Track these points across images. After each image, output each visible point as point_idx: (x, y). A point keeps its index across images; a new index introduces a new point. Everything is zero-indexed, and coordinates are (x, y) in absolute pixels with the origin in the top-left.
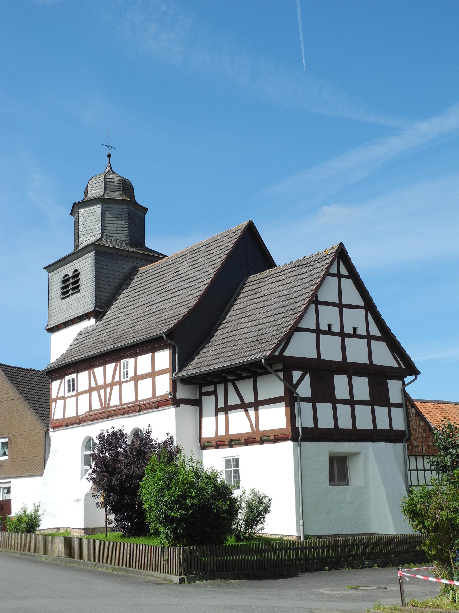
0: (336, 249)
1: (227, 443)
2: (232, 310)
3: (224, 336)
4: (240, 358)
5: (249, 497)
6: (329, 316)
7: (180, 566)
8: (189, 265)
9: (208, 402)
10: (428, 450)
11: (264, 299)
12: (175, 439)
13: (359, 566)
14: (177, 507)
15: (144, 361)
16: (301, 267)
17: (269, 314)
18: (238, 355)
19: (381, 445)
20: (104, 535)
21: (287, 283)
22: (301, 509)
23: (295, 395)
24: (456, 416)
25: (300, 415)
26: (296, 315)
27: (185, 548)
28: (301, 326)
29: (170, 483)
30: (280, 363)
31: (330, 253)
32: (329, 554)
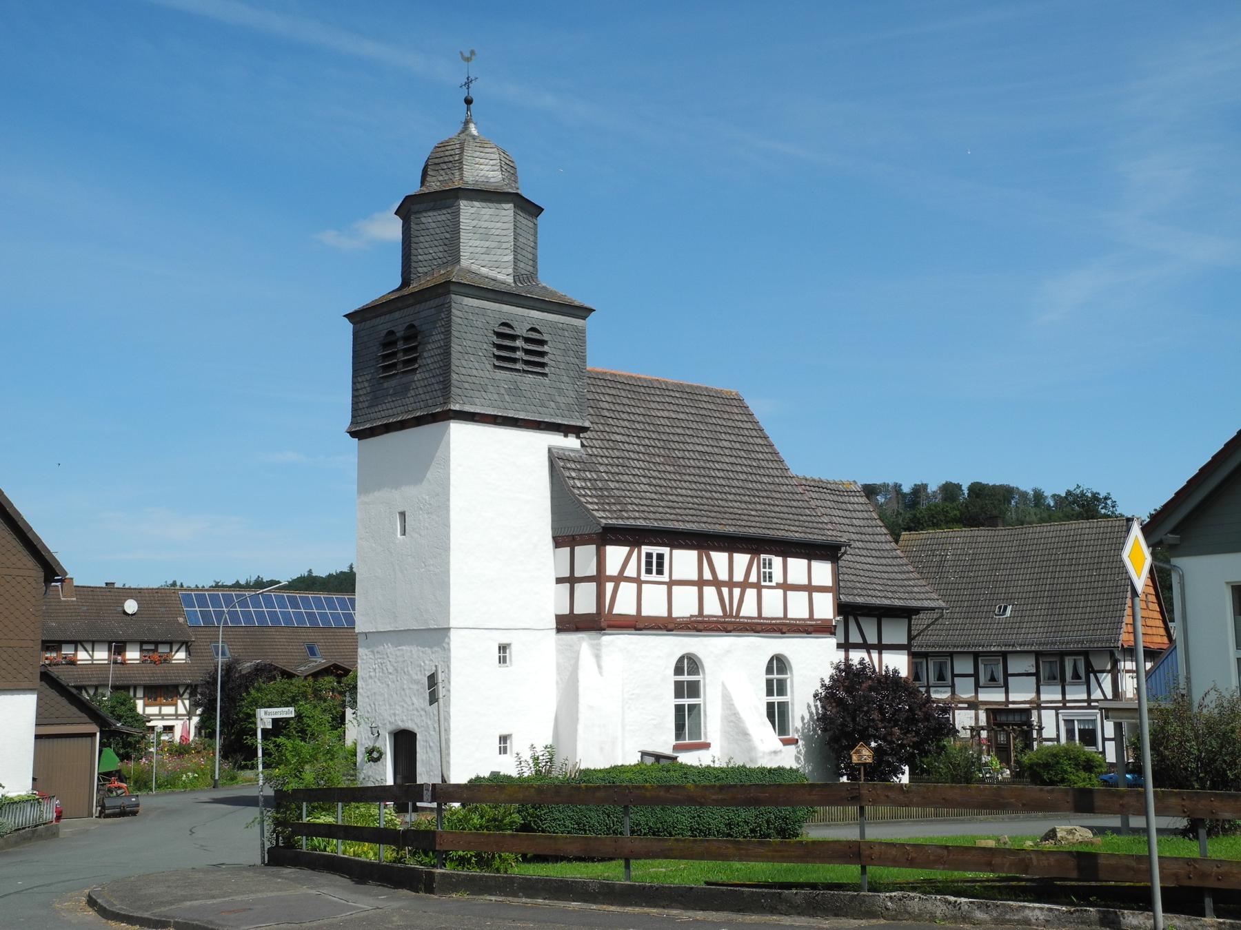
15: (797, 568)
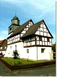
15: (17, 36)
20: (34, 42)
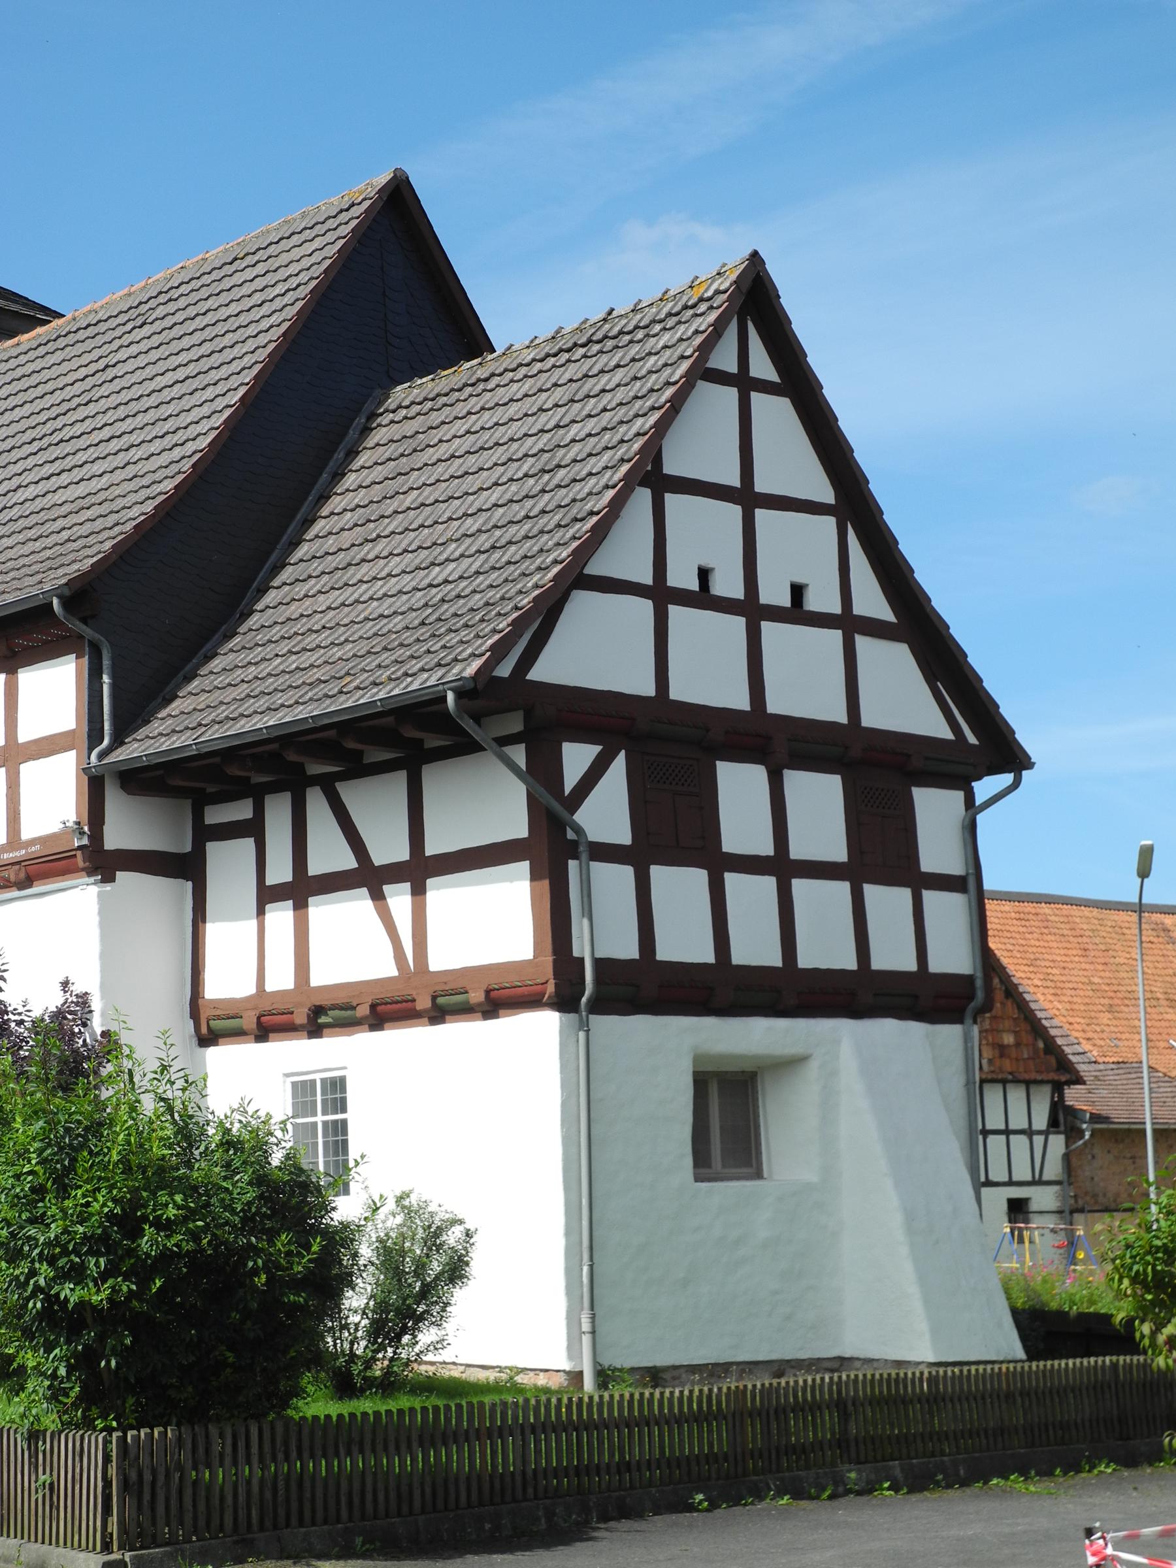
0: (733, 276)
1: (300, 1018)
2: (325, 511)
3: (294, 610)
4: (358, 688)
5: (389, 1224)
6: (703, 537)
7: (107, 1510)
8: (155, 341)
9: (229, 864)
10: (998, 1062)
11: (451, 471)
12: (96, 1004)
13: (824, 1489)
14: (97, 1264)
16: (596, 348)
17: (472, 525)
18: (348, 679)
19: (886, 1028)
21: (541, 410)
22: (585, 1269)
23: (571, 835)
24: (1090, 947)
25: (588, 912)
26: (578, 525)
27: (130, 1434)
28: (597, 567)
29: (71, 1168)
30: (510, 710)
31: (709, 294)
32: (711, 1445)
